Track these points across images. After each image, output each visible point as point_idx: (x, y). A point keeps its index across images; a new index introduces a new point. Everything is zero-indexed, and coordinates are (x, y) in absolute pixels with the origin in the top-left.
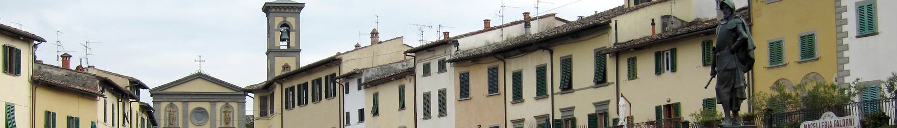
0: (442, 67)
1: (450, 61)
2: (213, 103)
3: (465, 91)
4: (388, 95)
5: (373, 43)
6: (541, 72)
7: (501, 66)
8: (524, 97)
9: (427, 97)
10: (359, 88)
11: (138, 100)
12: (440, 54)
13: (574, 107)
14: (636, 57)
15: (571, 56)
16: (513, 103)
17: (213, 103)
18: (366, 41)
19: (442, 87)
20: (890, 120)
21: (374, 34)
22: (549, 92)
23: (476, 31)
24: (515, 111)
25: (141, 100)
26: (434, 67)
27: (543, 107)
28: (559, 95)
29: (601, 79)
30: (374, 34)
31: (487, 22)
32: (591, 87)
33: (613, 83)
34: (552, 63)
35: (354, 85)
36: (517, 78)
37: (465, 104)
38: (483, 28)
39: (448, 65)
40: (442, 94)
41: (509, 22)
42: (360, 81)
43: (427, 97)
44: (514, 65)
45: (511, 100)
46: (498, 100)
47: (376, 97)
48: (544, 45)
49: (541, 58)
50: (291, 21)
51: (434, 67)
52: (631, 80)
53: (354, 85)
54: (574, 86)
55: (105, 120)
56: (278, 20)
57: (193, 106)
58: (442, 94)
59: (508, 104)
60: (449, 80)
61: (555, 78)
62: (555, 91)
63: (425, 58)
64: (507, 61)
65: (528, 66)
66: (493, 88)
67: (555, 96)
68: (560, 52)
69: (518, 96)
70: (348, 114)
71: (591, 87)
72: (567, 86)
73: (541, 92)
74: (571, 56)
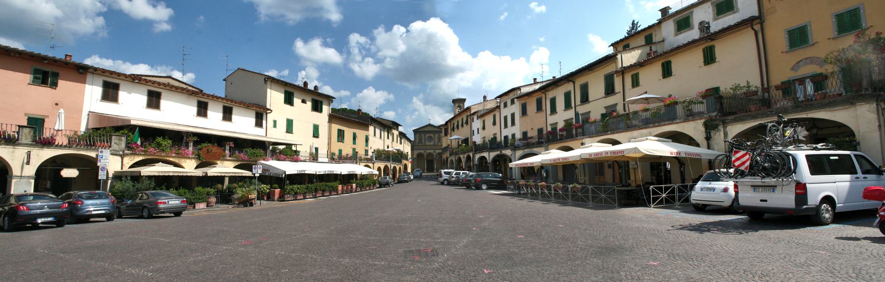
0: (513, 102)
1: (516, 98)
2: (434, 135)
3: (524, 112)
4: (489, 119)
5: (484, 101)
6: (567, 96)
7: (543, 95)
8: (557, 111)
9: (506, 118)
10: (478, 119)
11: (397, 130)
12: (511, 96)
13: (590, 112)
14: (638, 73)
15: (588, 82)
16: (550, 115)
17: (434, 135)
18: (482, 100)
19: (513, 133)
20: (577, 169)
21: (485, 97)
22: (573, 105)
23: (530, 83)
24: (551, 119)
25: (399, 130)
26: (509, 103)
27: (570, 114)
28: (580, 106)
29: (610, 90)
30: (485, 97)
31: (535, 79)
32: (603, 98)
33: (620, 92)
34: (574, 89)
35: (475, 117)
36: (553, 101)
37: (524, 118)
38: (533, 83)
39: (516, 100)
40: (513, 115)
41: (546, 80)
42: (477, 116)
43: (506, 118)
44: (550, 94)
45: (550, 113)
46: (542, 114)
47: (484, 121)
48: (570, 79)
49: (569, 87)
50: (461, 105)
51: (509, 103)
52: (634, 87)
53: (475, 117)
54: (590, 99)
55: (375, 135)
56: (457, 105)
57: (427, 135)
58: (513, 115)
59: (548, 116)
60: (516, 109)
61: (577, 97)
62: (577, 104)
63: (505, 98)
64: (547, 93)
65: (559, 94)
66: (539, 108)
67: (577, 107)
68: (580, 81)
69: (554, 111)
70: (473, 131)
71: (603, 98)
72: (585, 99)
73: (568, 106)
74: (588, 82)
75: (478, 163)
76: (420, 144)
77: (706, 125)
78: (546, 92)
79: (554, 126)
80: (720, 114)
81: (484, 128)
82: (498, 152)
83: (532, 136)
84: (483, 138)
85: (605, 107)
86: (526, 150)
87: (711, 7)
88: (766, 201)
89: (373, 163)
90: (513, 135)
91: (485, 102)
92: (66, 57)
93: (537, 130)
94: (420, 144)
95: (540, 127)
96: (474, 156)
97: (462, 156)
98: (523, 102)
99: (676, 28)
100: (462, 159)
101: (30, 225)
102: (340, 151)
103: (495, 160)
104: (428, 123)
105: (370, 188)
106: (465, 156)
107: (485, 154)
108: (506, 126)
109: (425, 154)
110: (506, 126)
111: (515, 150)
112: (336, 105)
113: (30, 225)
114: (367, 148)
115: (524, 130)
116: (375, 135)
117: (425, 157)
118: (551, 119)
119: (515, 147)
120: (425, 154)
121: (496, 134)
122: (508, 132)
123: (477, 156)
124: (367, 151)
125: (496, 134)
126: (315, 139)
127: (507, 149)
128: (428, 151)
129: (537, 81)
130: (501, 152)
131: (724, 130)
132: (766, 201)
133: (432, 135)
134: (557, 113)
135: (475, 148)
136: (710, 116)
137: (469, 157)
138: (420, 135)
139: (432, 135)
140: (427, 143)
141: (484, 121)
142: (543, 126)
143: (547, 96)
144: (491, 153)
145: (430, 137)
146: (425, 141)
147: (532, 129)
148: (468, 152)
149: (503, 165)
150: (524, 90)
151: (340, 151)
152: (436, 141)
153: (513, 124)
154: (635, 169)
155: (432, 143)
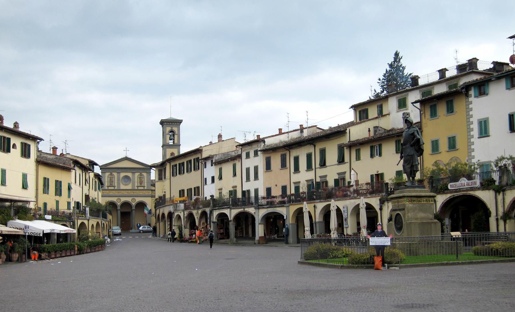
0: (256, 154)
1: (260, 151)
3: (268, 167)
4: (227, 169)
5: (219, 141)
6: (309, 157)
9: (248, 170)
11: (93, 172)
12: (255, 147)
16: (294, 173)
21: (220, 136)
24: (295, 178)
25: (95, 172)
26: (252, 154)
27: (310, 175)
29: (341, 160)
30: (220, 136)
31: (280, 130)
32: (336, 165)
33: (348, 162)
34: (315, 151)
36: (296, 159)
37: (269, 173)
39: (259, 153)
40: (256, 168)
41: (292, 130)
42: (212, 161)
43: (248, 170)
44: (295, 153)
45: (293, 171)
47: (221, 170)
48: (311, 142)
49: (310, 149)
50: (175, 129)
51: (252, 154)
54: (327, 164)
55: (76, 182)
56: (168, 129)
57: (122, 175)
58: (256, 168)
59: (292, 174)
60: (260, 161)
61: (316, 160)
62: (317, 167)
63: (247, 149)
65: (302, 154)
66: (284, 165)
68: (320, 146)
69: (297, 169)
70: (206, 179)
71: (336, 165)
72: (323, 164)
73: (309, 167)
75: (216, 221)
76: (110, 188)
77: (380, 200)
78: (290, 149)
79: (297, 185)
80: (386, 195)
81: (220, 178)
82: (243, 210)
83: (274, 195)
84: (219, 190)
85: (337, 173)
86: (269, 209)
87: (419, 94)
88: (25, 176)
89: (88, 220)
90: (256, 191)
91: (220, 143)
92: (138, 188)
93: (281, 188)
94: (110, 188)
95: (284, 184)
96: (211, 212)
97: (194, 212)
98: (268, 155)
99: (398, 106)
100: (195, 214)
101: (136, 237)
102: (45, 204)
103: (237, 217)
104: (123, 156)
105: (61, 254)
106: (200, 212)
107: (227, 211)
108: (248, 179)
109: (119, 204)
110: (248, 179)
111: (259, 209)
112: (45, 147)
113: (136, 237)
114: (69, 200)
115: (269, 186)
116: (76, 182)
117: (119, 208)
118: (295, 178)
119: (259, 205)
120: (119, 204)
121: (236, 187)
122: (250, 186)
123: (216, 213)
124: (69, 204)
125: (236, 187)
126: (24, 190)
127: (251, 207)
128: (123, 199)
129: (283, 132)
130: (244, 209)
131: (388, 205)
132: (25, 176)
133: (130, 174)
134: (300, 172)
135: (213, 203)
136: (382, 195)
137: (204, 214)
138: (111, 174)
139: (130, 174)
140: (122, 187)
141: (221, 170)
142: (287, 183)
143: (291, 153)
144: (232, 210)
145: (127, 177)
146: (119, 184)
147: (276, 185)
148: (204, 207)
149: (244, 222)
150: (269, 142)
151: (45, 204)
152: (136, 185)
153: (256, 177)
154: (347, 228)
155: (129, 187)
